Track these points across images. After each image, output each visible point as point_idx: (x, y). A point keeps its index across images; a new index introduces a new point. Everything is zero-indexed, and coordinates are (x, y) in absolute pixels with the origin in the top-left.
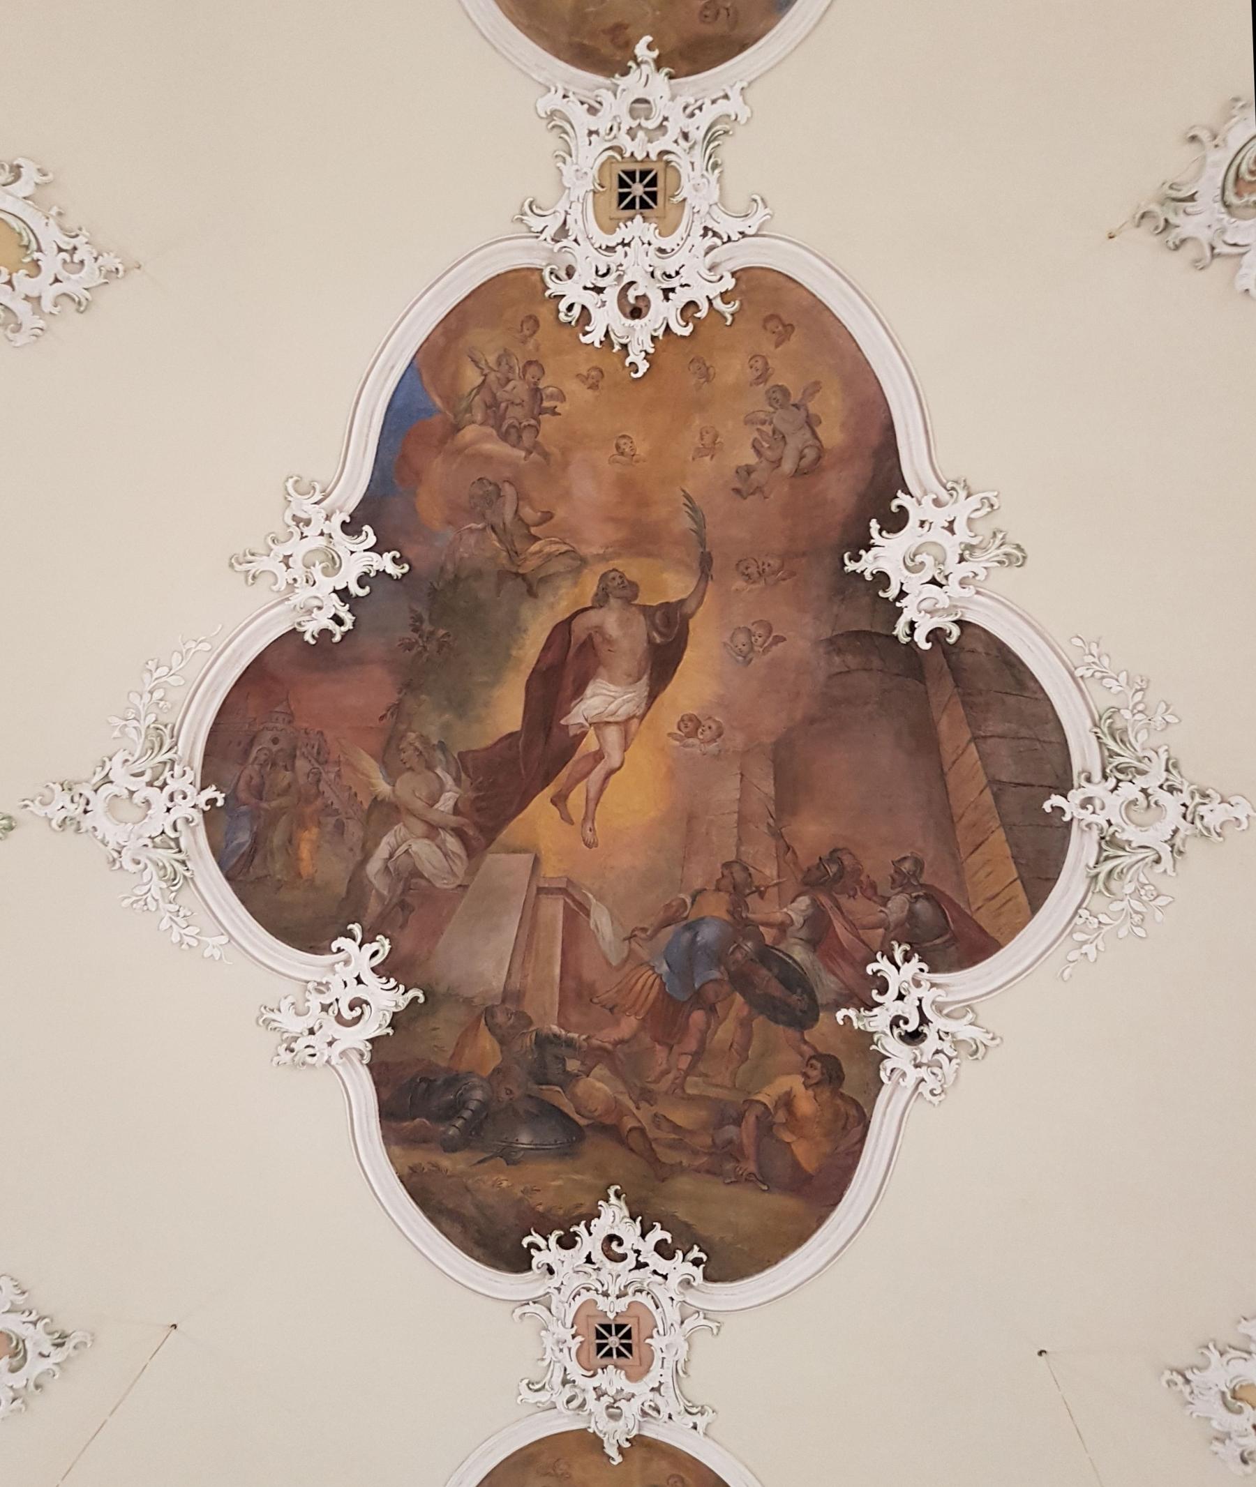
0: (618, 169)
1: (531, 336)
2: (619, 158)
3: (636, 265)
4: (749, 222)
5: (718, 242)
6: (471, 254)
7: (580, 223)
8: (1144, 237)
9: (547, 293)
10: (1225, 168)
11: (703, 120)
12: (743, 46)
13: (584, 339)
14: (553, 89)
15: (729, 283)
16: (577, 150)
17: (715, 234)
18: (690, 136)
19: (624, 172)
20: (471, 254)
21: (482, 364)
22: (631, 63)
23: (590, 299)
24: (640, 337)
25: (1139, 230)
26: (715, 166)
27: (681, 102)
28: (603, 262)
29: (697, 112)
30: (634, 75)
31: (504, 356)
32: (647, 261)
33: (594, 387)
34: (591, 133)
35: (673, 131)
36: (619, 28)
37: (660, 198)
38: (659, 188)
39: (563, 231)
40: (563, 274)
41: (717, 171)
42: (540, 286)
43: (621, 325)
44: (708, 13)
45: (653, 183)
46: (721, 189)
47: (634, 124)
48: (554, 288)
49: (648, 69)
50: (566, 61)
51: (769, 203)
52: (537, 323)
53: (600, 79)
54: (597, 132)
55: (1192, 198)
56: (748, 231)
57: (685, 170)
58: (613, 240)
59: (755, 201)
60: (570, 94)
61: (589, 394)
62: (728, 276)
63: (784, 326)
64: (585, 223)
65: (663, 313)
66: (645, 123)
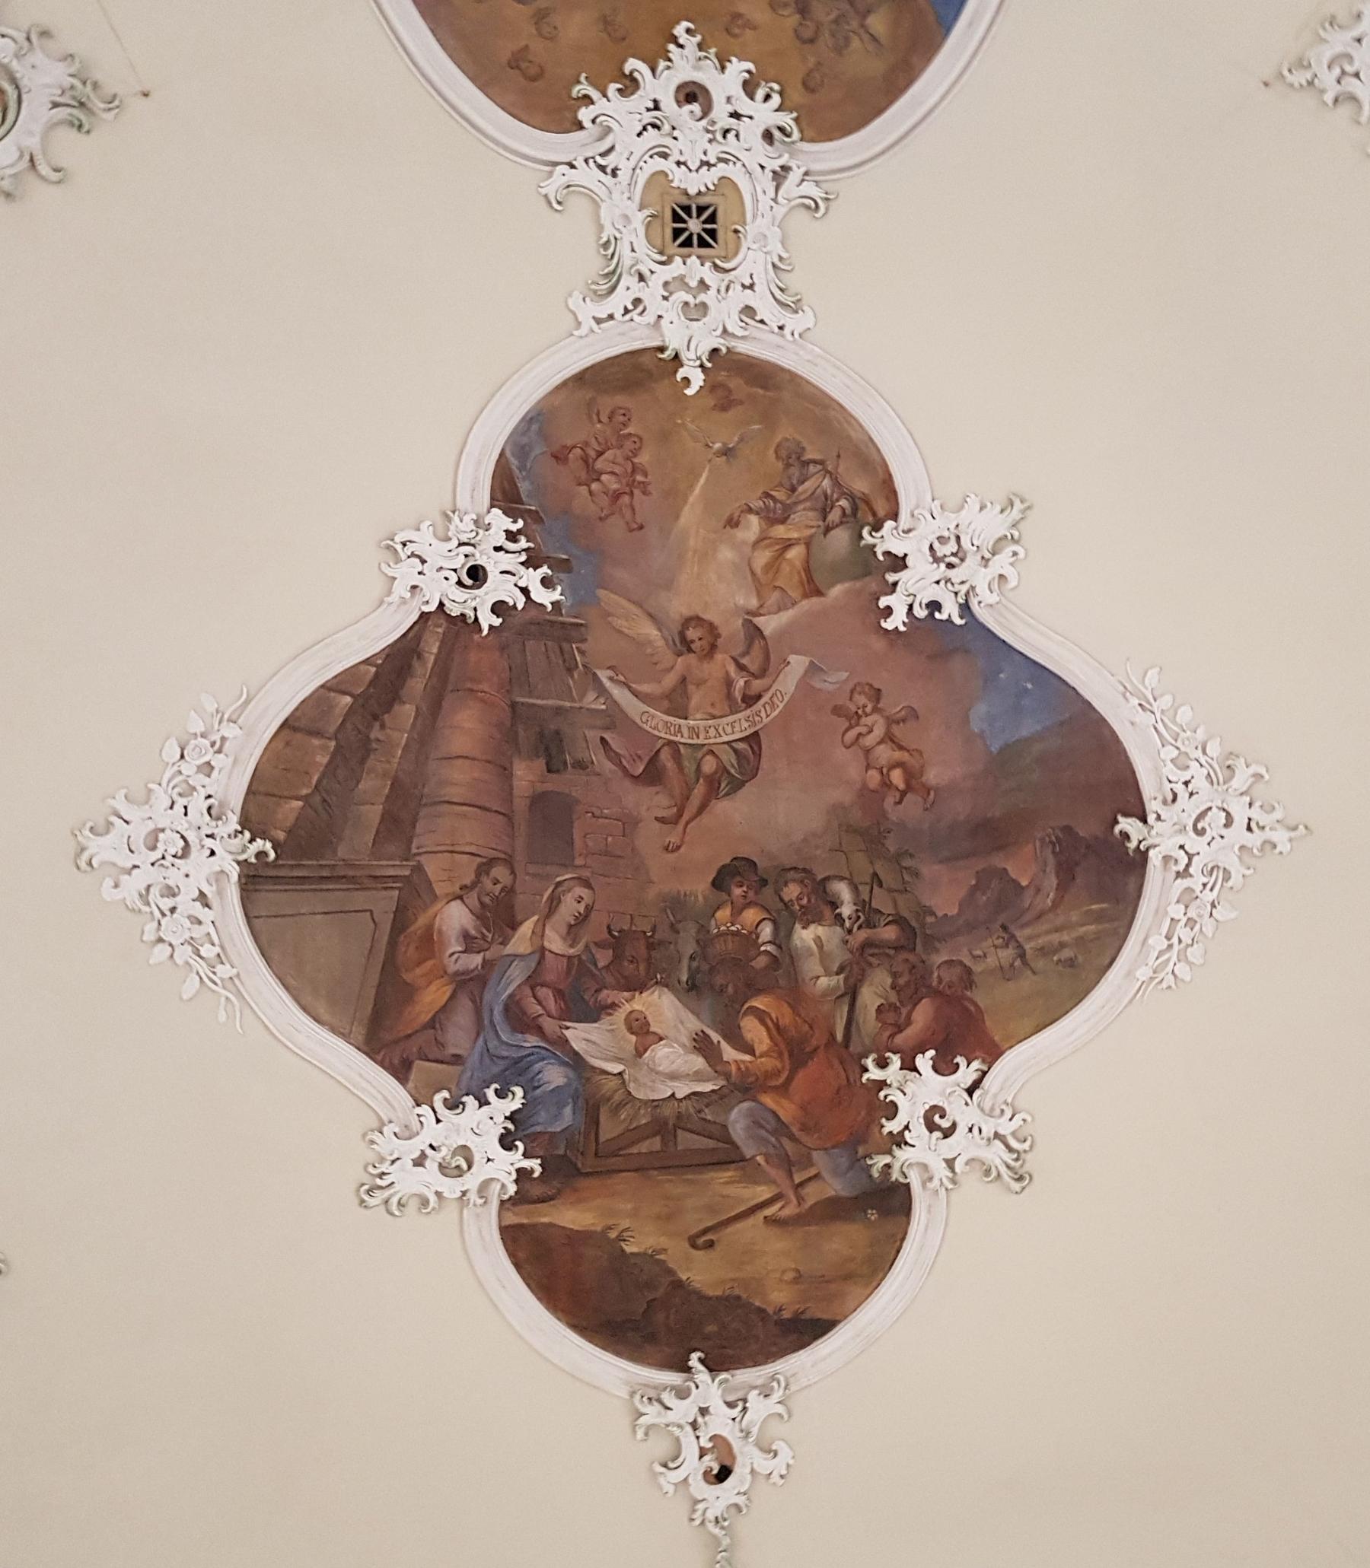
0: (718, 250)
1: (811, 71)
2: (718, 262)
3: (690, 135)
4: (564, 180)
5: (599, 159)
6: (883, 153)
7: (759, 189)
8: (111, 74)
9: (795, 115)
10: (19, 123)
11: (621, 298)
12: (581, 379)
13: (750, 66)
14: (796, 336)
15: (585, 114)
16: (766, 269)
17: (602, 168)
18: (636, 278)
19: (710, 246)
20: (883, 153)
21: (866, 37)
22: (709, 365)
23: (744, 105)
24: (686, 62)
25: (113, 92)
26: (606, 245)
27: (650, 318)
28: (731, 144)
29: (630, 307)
30: (704, 350)
31: (840, 49)
32: (679, 145)
33: (737, 16)
34: (751, 287)
35: (656, 283)
36: (724, 406)
37: (668, 215)
38: (670, 226)
39: (780, 175)
40: (777, 134)
41: (605, 239)
42: (804, 124)
43: (706, 75)
44: (622, 418)
45: (677, 233)
46: (598, 217)
47: (702, 297)
48: (787, 119)
49: (686, 356)
50: (782, 369)
51: (543, 201)
52: (805, 84)
53: (742, 347)
54: (743, 286)
55: (55, 105)
56: (565, 168)
57: (641, 244)
58: (721, 169)
59: (559, 203)
60: (776, 330)
61: (742, 8)
62: (587, 124)
63: (518, 67)
64: (754, 189)
65: (659, 86)
66: (689, 298)
